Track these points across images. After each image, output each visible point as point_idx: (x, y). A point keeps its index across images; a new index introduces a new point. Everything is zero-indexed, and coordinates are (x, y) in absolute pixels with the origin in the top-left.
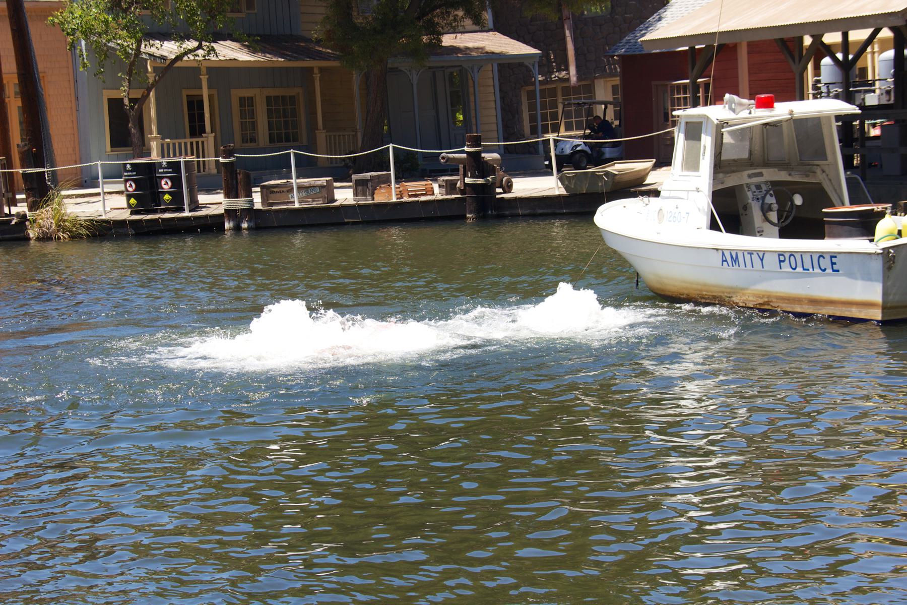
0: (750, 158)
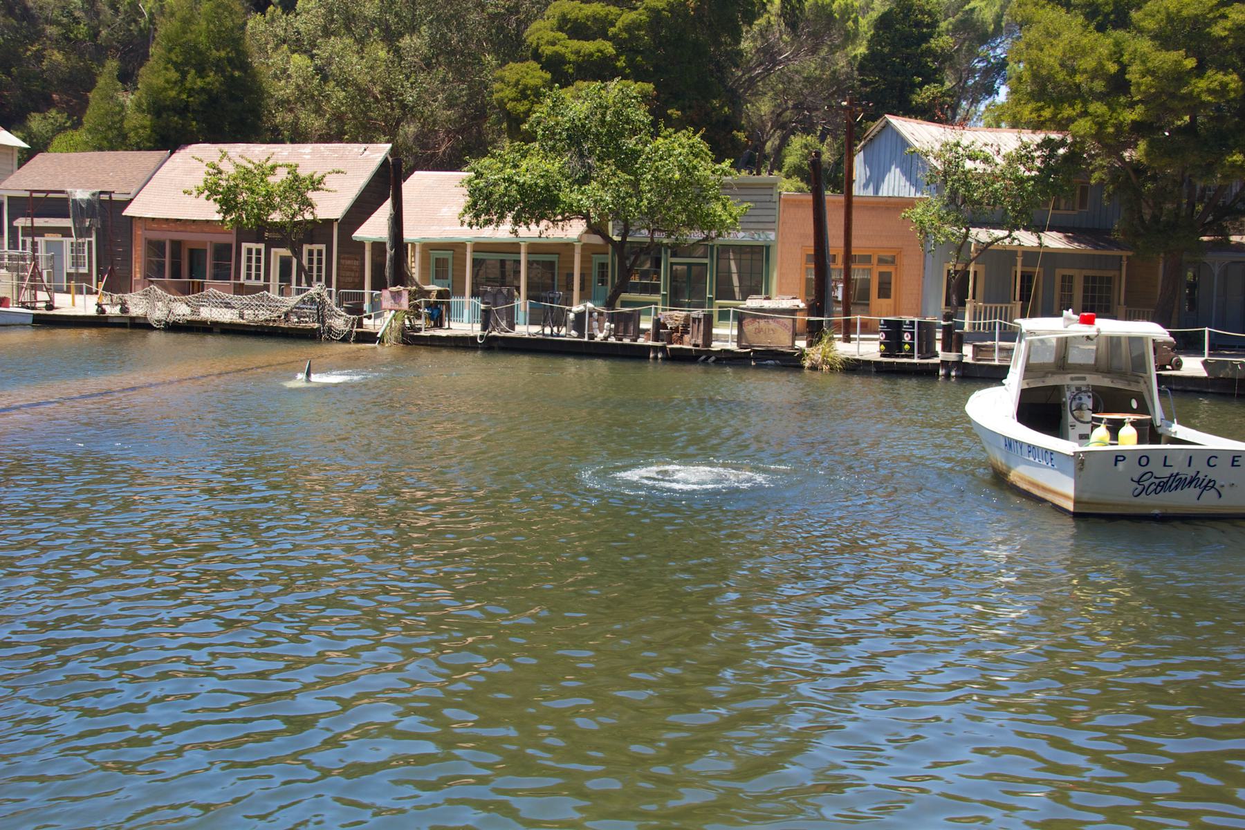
0: (1095, 365)
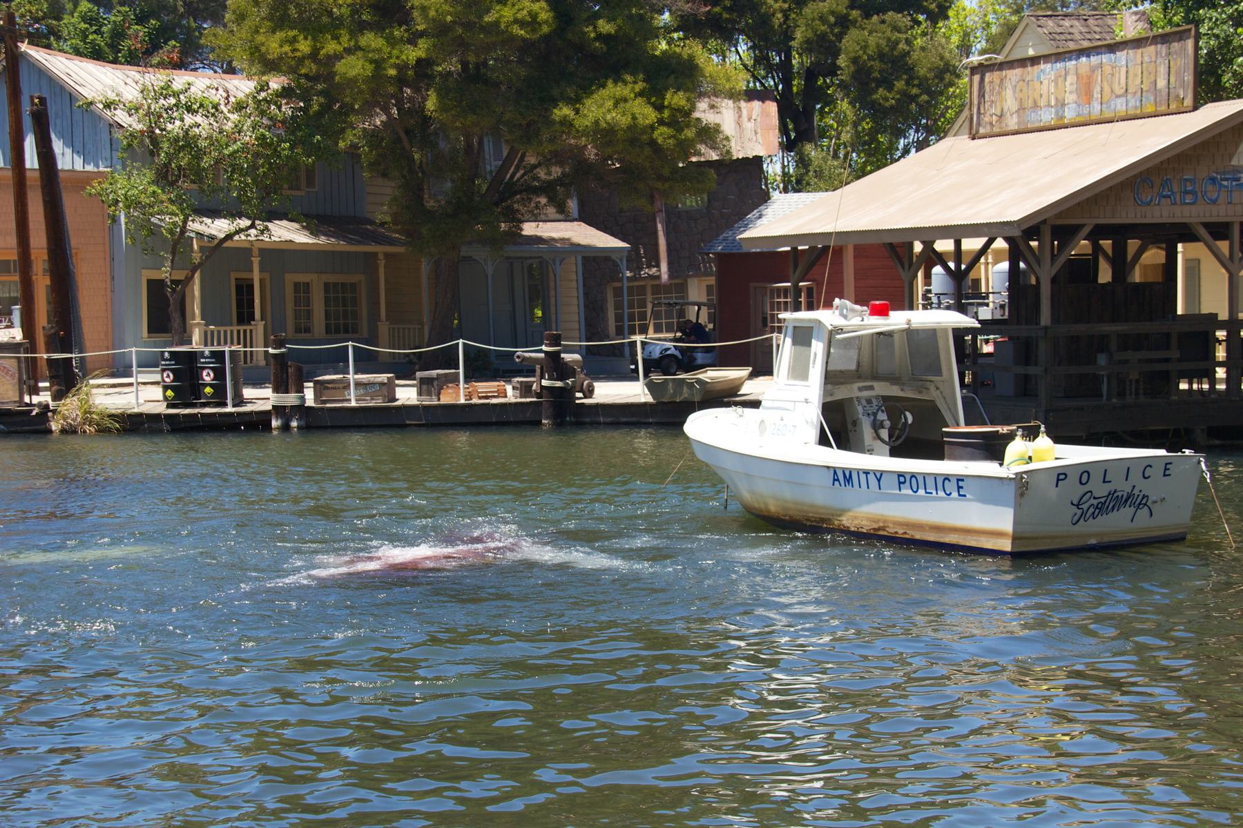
0: (857, 370)
